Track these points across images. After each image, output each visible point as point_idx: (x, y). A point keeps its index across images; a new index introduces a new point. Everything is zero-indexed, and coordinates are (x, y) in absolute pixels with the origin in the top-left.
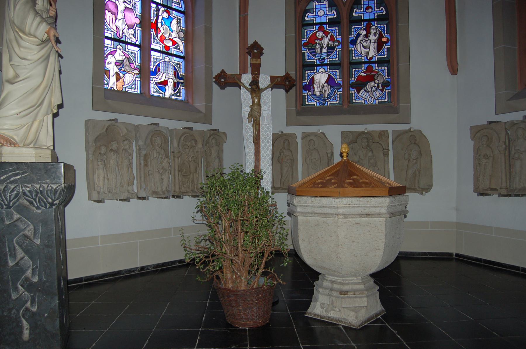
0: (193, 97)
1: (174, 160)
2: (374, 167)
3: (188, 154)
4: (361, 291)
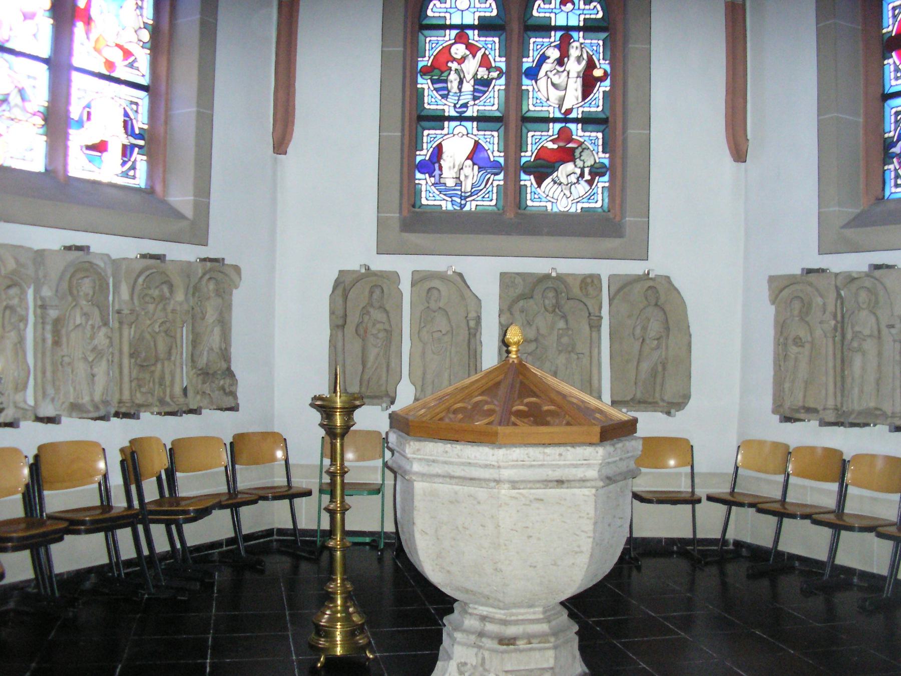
0: (164, 181)
1: (120, 329)
2: (570, 352)
3: (154, 315)
4: (542, 637)
